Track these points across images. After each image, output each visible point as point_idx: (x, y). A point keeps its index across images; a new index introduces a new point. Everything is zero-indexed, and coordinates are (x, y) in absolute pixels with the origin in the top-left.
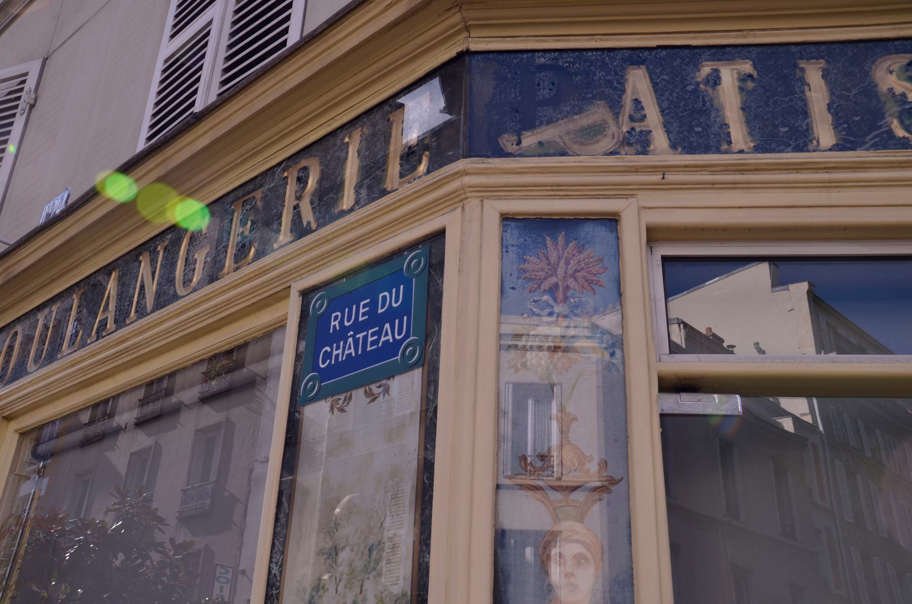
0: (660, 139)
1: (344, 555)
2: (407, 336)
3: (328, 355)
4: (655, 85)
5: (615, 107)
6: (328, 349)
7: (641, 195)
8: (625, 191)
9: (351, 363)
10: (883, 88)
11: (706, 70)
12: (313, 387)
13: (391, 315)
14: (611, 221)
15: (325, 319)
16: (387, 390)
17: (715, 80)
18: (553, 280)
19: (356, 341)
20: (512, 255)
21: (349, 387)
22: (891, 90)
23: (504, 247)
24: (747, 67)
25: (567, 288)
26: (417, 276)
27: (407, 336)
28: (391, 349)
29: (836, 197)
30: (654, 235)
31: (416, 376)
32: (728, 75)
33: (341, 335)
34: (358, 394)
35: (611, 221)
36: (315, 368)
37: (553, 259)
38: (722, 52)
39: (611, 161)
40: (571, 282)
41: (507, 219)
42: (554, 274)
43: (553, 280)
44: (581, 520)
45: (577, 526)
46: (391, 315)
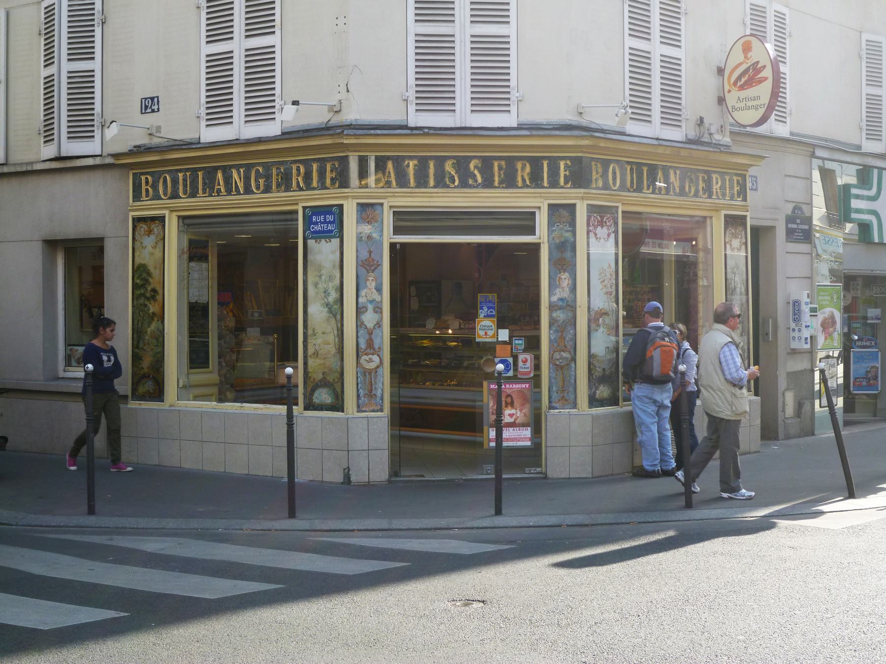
0: (394, 183)
1: (323, 277)
2: (335, 229)
3: (313, 228)
4: (394, 167)
5: (384, 174)
6: (313, 226)
7: (389, 198)
8: (385, 198)
9: (319, 232)
10: (446, 170)
11: (406, 162)
12: (310, 235)
13: (330, 222)
14: (382, 204)
15: (311, 218)
16: (330, 241)
17: (408, 166)
18: (368, 220)
19: (321, 226)
20: (359, 213)
21: (321, 238)
22: (448, 171)
23: (357, 211)
24: (416, 162)
25: (371, 222)
26: (337, 214)
27: (335, 229)
28: (331, 231)
29: (431, 200)
30: (391, 207)
31: (336, 242)
32: (412, 164)
33: (316, 223)
34: (323, 240)
35: (382, 204)
36: (310, 230)
37: (368, 214)
38: (411, 158)
39: (382, 190)
40: (372, 220)
41: (358, 204)
42: (368, 218)
43: (368, 220)
44: (373, 273)
45: (372, 274)
46: (330, 222)
